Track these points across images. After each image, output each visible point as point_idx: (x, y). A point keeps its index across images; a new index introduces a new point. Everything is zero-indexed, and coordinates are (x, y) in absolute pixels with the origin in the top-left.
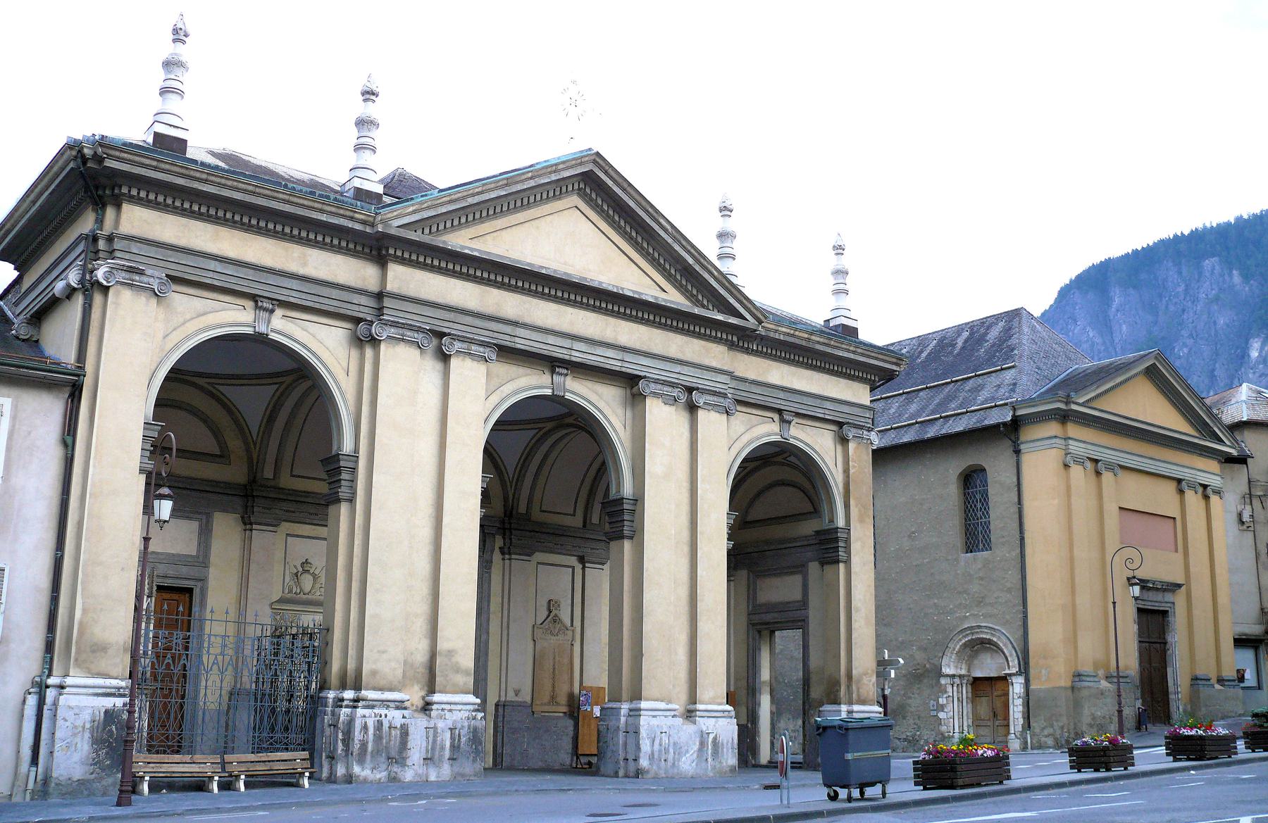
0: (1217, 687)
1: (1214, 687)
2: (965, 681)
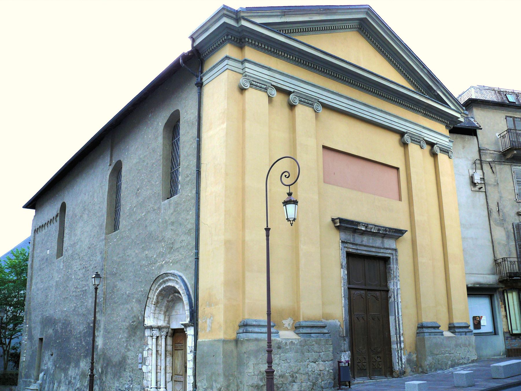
0: (447, 334)
1: (442, 335)
2: (164, 333)
